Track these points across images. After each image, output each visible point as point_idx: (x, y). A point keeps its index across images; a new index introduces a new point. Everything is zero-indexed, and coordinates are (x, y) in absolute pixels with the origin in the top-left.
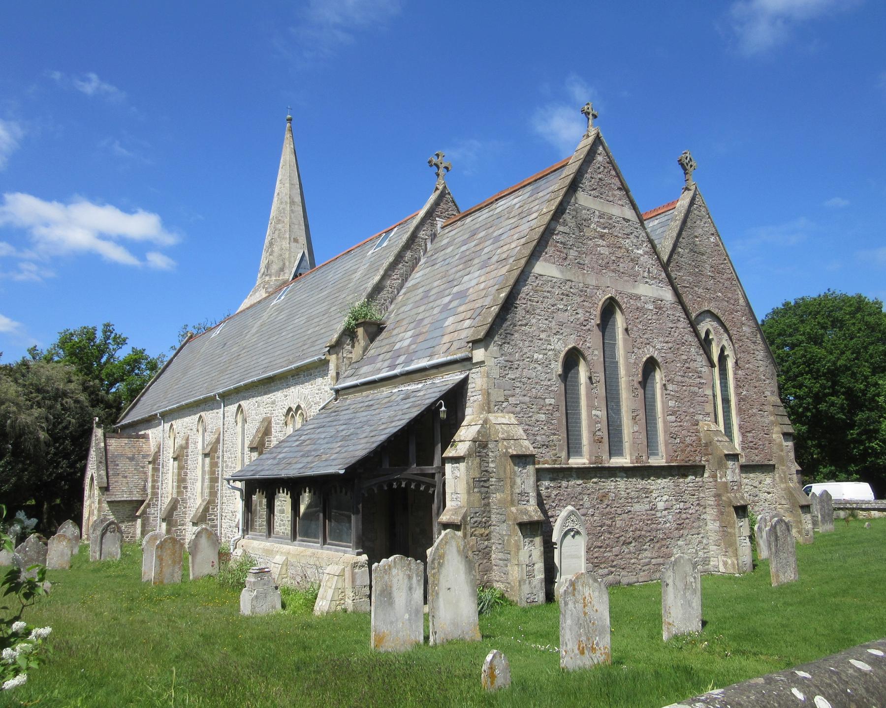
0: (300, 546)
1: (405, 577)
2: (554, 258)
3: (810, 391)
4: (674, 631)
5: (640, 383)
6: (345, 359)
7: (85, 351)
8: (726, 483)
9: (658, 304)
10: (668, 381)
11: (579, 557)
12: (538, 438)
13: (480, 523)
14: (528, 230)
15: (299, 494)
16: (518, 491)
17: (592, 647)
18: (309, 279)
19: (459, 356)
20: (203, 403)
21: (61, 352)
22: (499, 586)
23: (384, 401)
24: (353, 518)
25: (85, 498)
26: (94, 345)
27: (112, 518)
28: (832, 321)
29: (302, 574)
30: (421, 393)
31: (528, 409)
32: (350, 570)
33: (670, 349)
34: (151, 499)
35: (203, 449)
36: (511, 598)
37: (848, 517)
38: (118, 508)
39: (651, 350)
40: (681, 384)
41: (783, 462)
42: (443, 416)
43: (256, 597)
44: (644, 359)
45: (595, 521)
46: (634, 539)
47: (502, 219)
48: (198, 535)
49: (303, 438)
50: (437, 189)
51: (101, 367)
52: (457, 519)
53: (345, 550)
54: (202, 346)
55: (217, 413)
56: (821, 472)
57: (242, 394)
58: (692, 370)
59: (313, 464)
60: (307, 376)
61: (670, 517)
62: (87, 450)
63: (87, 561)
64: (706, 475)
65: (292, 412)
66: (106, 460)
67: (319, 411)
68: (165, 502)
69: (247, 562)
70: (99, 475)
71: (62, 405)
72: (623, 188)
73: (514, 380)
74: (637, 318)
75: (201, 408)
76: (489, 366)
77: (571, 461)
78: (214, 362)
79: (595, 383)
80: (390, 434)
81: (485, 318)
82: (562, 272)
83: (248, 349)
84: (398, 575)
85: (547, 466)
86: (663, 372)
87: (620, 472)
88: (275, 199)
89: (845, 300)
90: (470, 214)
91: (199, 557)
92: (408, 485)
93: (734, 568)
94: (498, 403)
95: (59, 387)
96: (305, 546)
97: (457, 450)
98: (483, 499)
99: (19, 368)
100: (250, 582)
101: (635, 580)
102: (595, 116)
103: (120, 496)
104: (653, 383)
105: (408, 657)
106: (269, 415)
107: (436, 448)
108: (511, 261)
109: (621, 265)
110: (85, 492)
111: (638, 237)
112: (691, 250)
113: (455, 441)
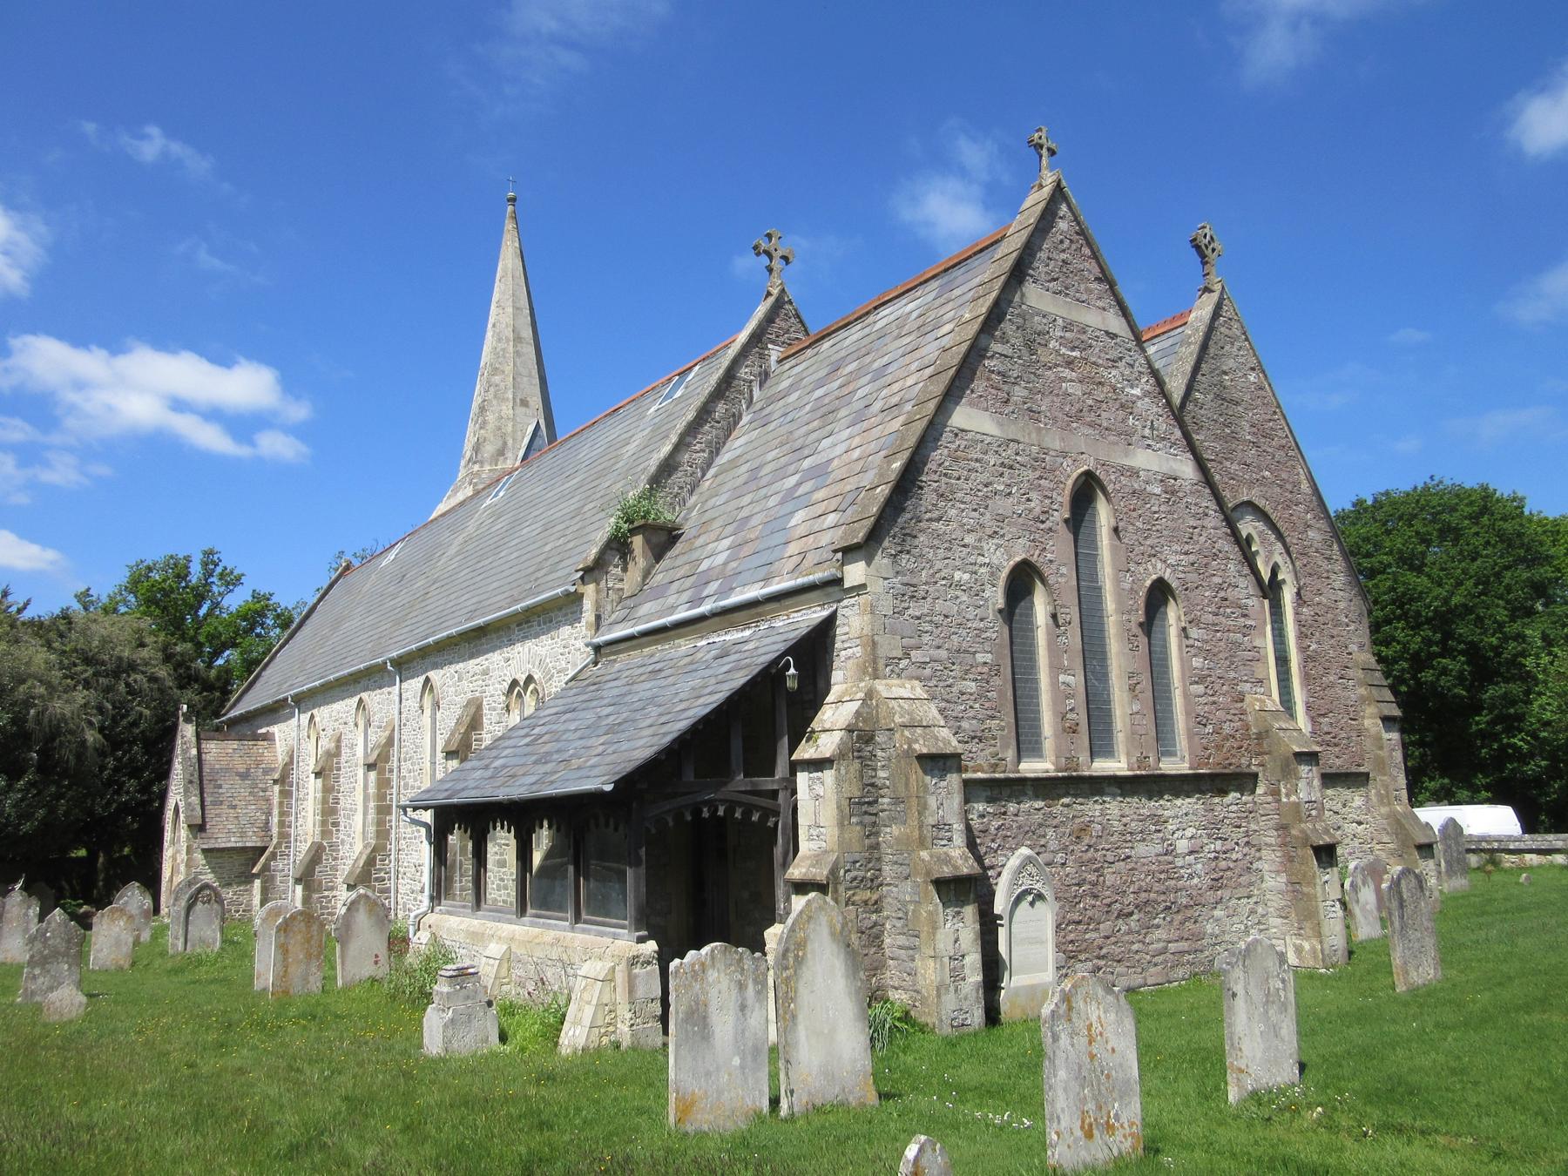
0: (532, 925)
1: (733, 985)
2: (987, 400)
3: (1405, 648)
4: (1249, 1085)
5: (1141, 625)
6: (610, 592)
7: (173, 596)
8: (1297, 805)
9: (1168, 481)
10: (1190, 622)
11: (1043, 942)
12: (965, 724)
13: (862, 881)
14: (937, 353)
15: (531, 831)
16: (931, 821)
17: (1108, 1122)
18: (548, 461)
19: (818, 576)
20: (365, 676)
21: (131, 598)
22: (898, 997)
23: (682, 663)
24: (630, 872)
25: (166, 845)
26: (187, 587)
27: (209, 878)
28: (1440, 530)
29: (536, 978)
30: (751, 646)
31: (946, 672)
32: (625, 969)
33: (1192, 564)
34: (279, 844)
35: (364, 757)
36: (922, 1020)
37: (1484, 865)
38: (219, 861)
39: (1159, 568)
40: (1213, 628)
41: (1383, 768)
42: (792, 684)
43: (452, 1020)
44: (1148, 583)
45: (1067, 876)
46: (1136, 908)
47: (888, 339)
48: (352, 907)
49: (537, 731)
50: (769, 294)
51: (199, 624)
52: (820, 874)
53: (614, 934)
54: (365, 583)
55: (389, 693)
56: (1426, 789)
57: (433, 659)
58: (1232, 603)
59: (557, 776)
60: (545, 623)
61: (1199, 866)
62: (169, 762)
63: (163, 954)
64: (1259, 791)
65: (518, 688)
66: (200, 778)
67: (566, 683)
68: (301, 850)
69: (440, 954)
70: (188, 805)
71: (128, 685)
72: (1105, 278)
73: (919, 618)
74: (1134, 510)
75: (361, 685)
76: (875, 594)
77: (1023, 766)
78: (386, 606)
79: (1064, 625)
80: (696, 719)
81: (865, 507)
82: (1000, 425)
83: (443, 583)
84: (719, 982)
85: (980, 775)
86: (1181, 606)
87: (1109, 785)
88: (489, 334)
89: (1460, 494)
90: (829, 334)
91: (354, 947)
92: (730, 811)
93: (1315, 958)
94: (892, 661)
95: (122, 654)
96: (544, 926)
97: (818, 746)
98: (868, 836)
99: (54, 624)
100: (442, 993)
101: (1140, 981)
102: (1052, 152)
103: (224, 840)
104: (1163, 626)
105: (743, 1141)
106: (478, 694)
107: (779, 745)
108: (908, 407)
109: (1103, 414)
110: (166, 834)
111: (1132, 366)
112: (1217, 396)
113: (813, 732)
